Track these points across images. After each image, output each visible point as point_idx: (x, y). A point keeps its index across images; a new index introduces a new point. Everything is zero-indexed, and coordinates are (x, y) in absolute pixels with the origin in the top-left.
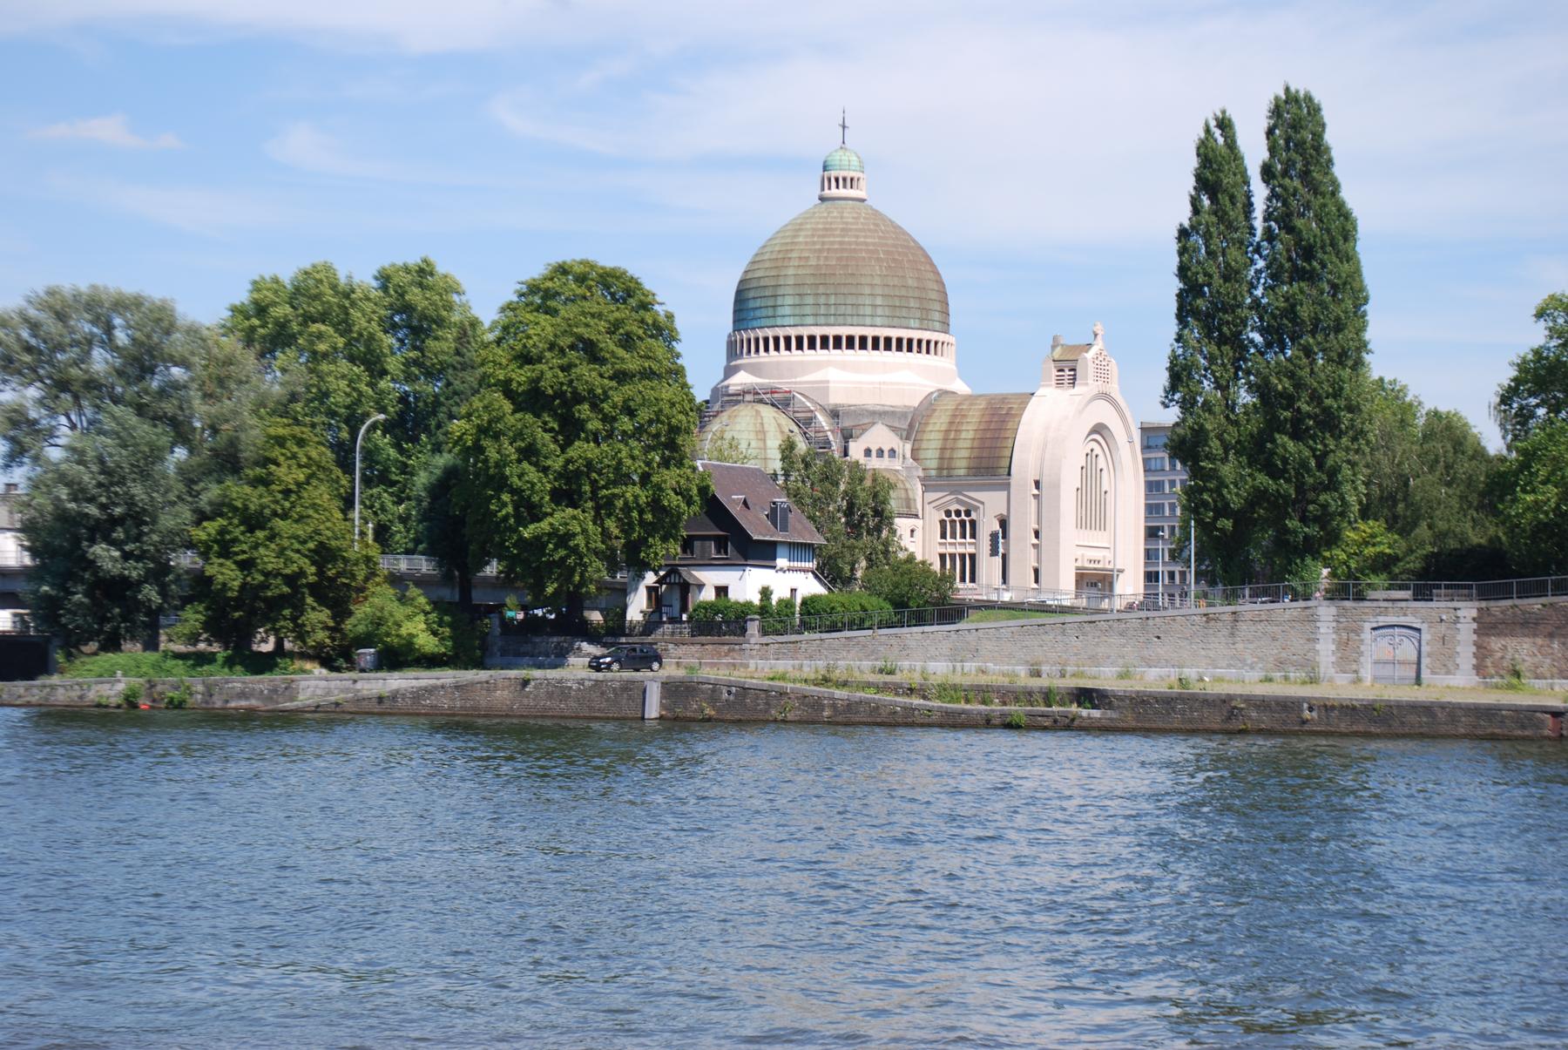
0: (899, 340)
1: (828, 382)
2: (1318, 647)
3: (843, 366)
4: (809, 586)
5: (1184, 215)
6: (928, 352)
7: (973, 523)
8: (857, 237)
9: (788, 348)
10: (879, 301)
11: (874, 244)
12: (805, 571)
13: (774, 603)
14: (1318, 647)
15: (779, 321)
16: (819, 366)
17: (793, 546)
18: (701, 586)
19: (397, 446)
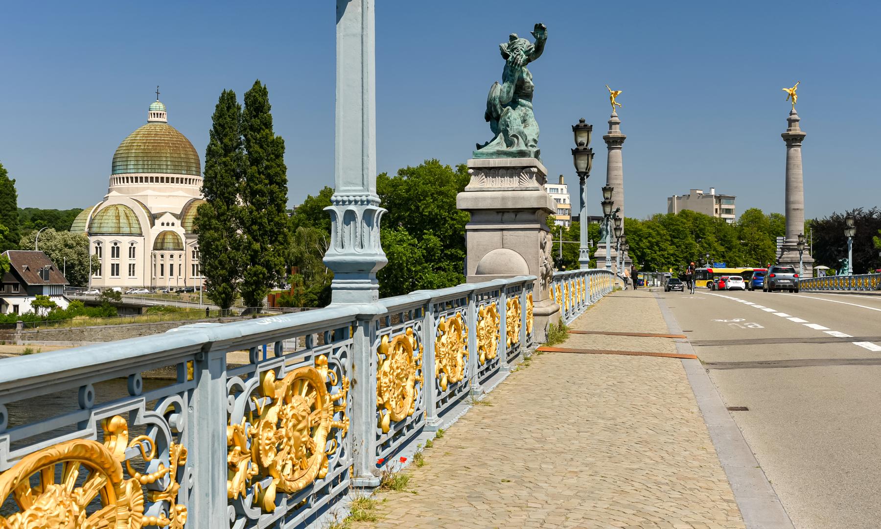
0: (177, 179)
3: (154, 189)
8: (161, 137)
10: (169, 163)
11: (168, 140)
15: (129, 171)
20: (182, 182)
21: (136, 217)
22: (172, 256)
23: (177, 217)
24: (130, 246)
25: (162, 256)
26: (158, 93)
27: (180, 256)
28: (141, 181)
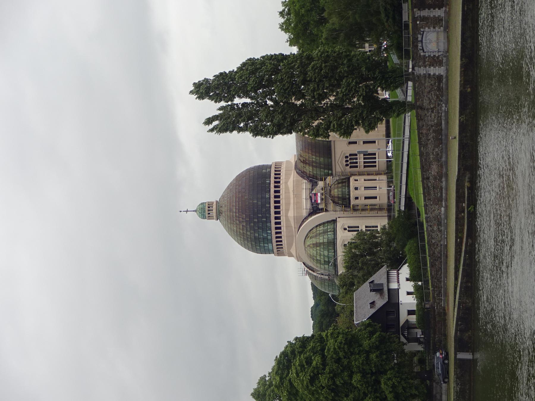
0: (275, 187)
1: (294, 216)
2: (432, 74)
3: (287, 210)
4: (405, 271)
5: (248, 135)
6: (280, 171)
7: (351, 155)
8: (233, 206)
9: (280, 233)
12: (398, 274)
13: (295, 50)
14: (432, 74)
16: (287, 220)
17: (388, 282)
18: (407, 321)
19: (310, 349)
20: (279, 182)
21: (317, 226)
22: (356, 189)
23: (314, 184)
24: (347, 231)
25: (357, 198)
26: (187, 211)
27: (356, 180)
28: (280, 228)
